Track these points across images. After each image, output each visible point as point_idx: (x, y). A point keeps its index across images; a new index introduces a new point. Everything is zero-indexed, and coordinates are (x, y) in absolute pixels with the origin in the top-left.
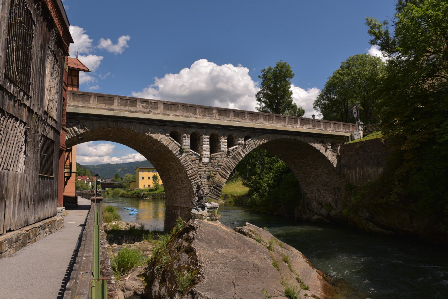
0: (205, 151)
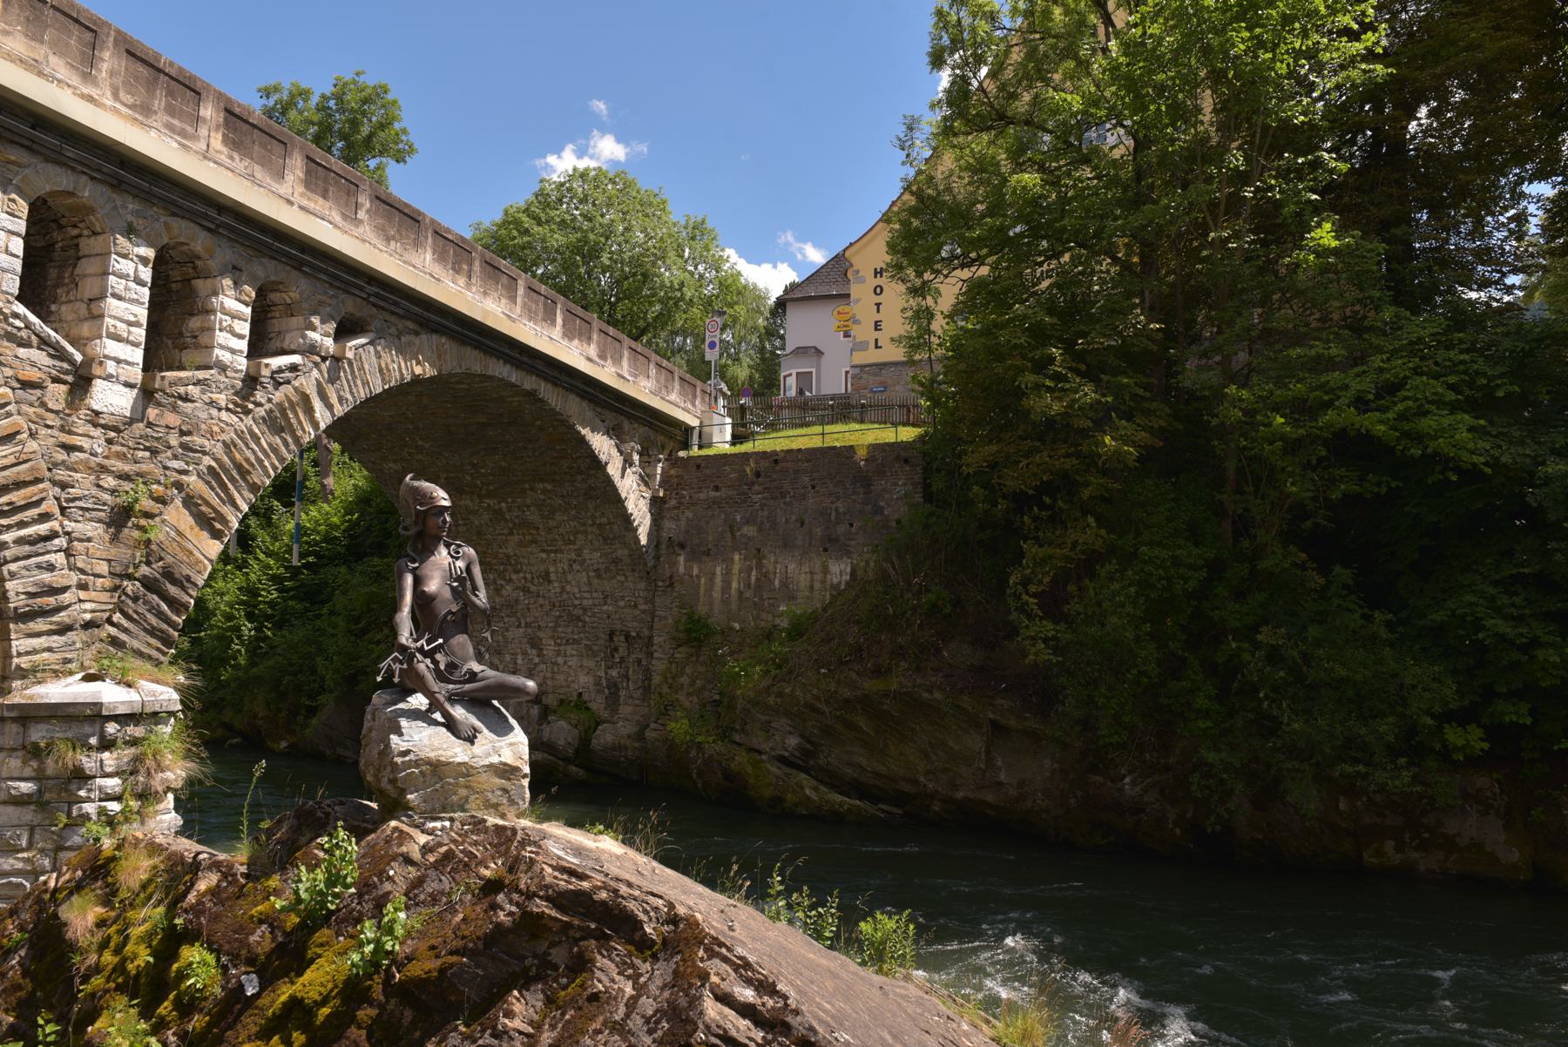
0: (118, 338)
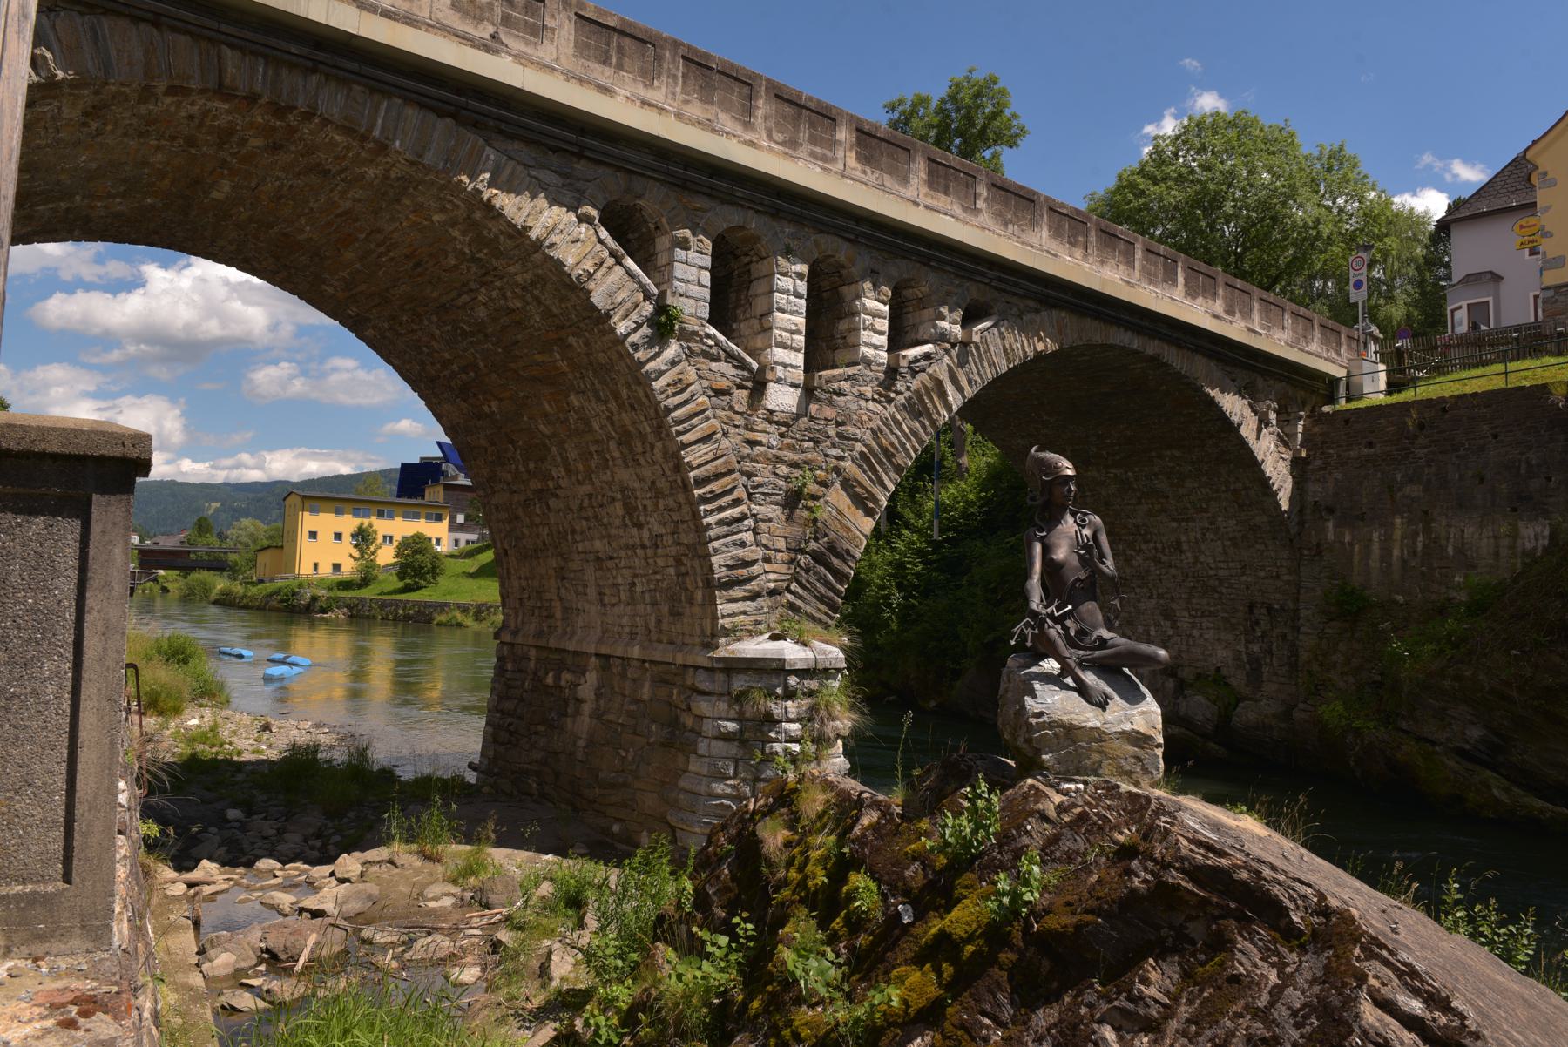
0: (784, 346)
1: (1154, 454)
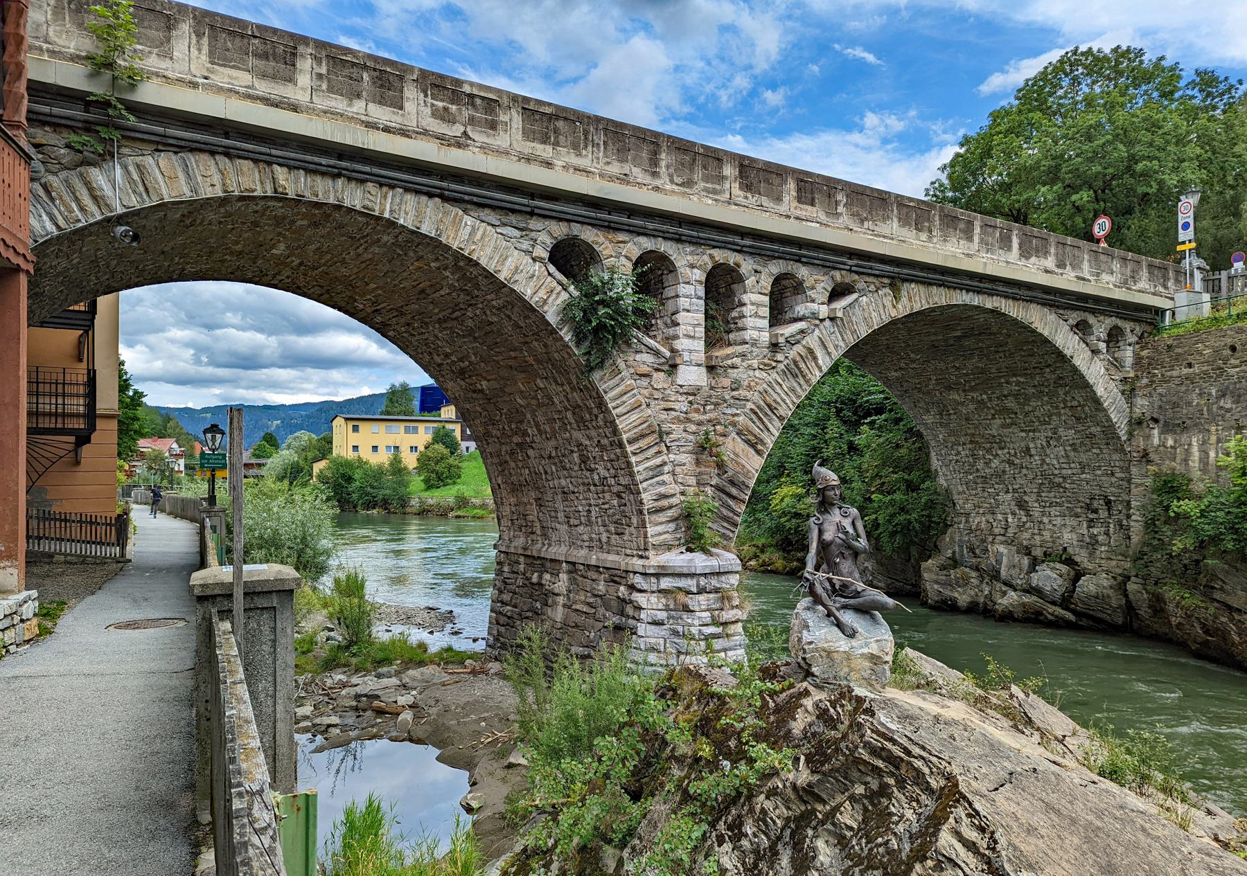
1: (1003, 380)
